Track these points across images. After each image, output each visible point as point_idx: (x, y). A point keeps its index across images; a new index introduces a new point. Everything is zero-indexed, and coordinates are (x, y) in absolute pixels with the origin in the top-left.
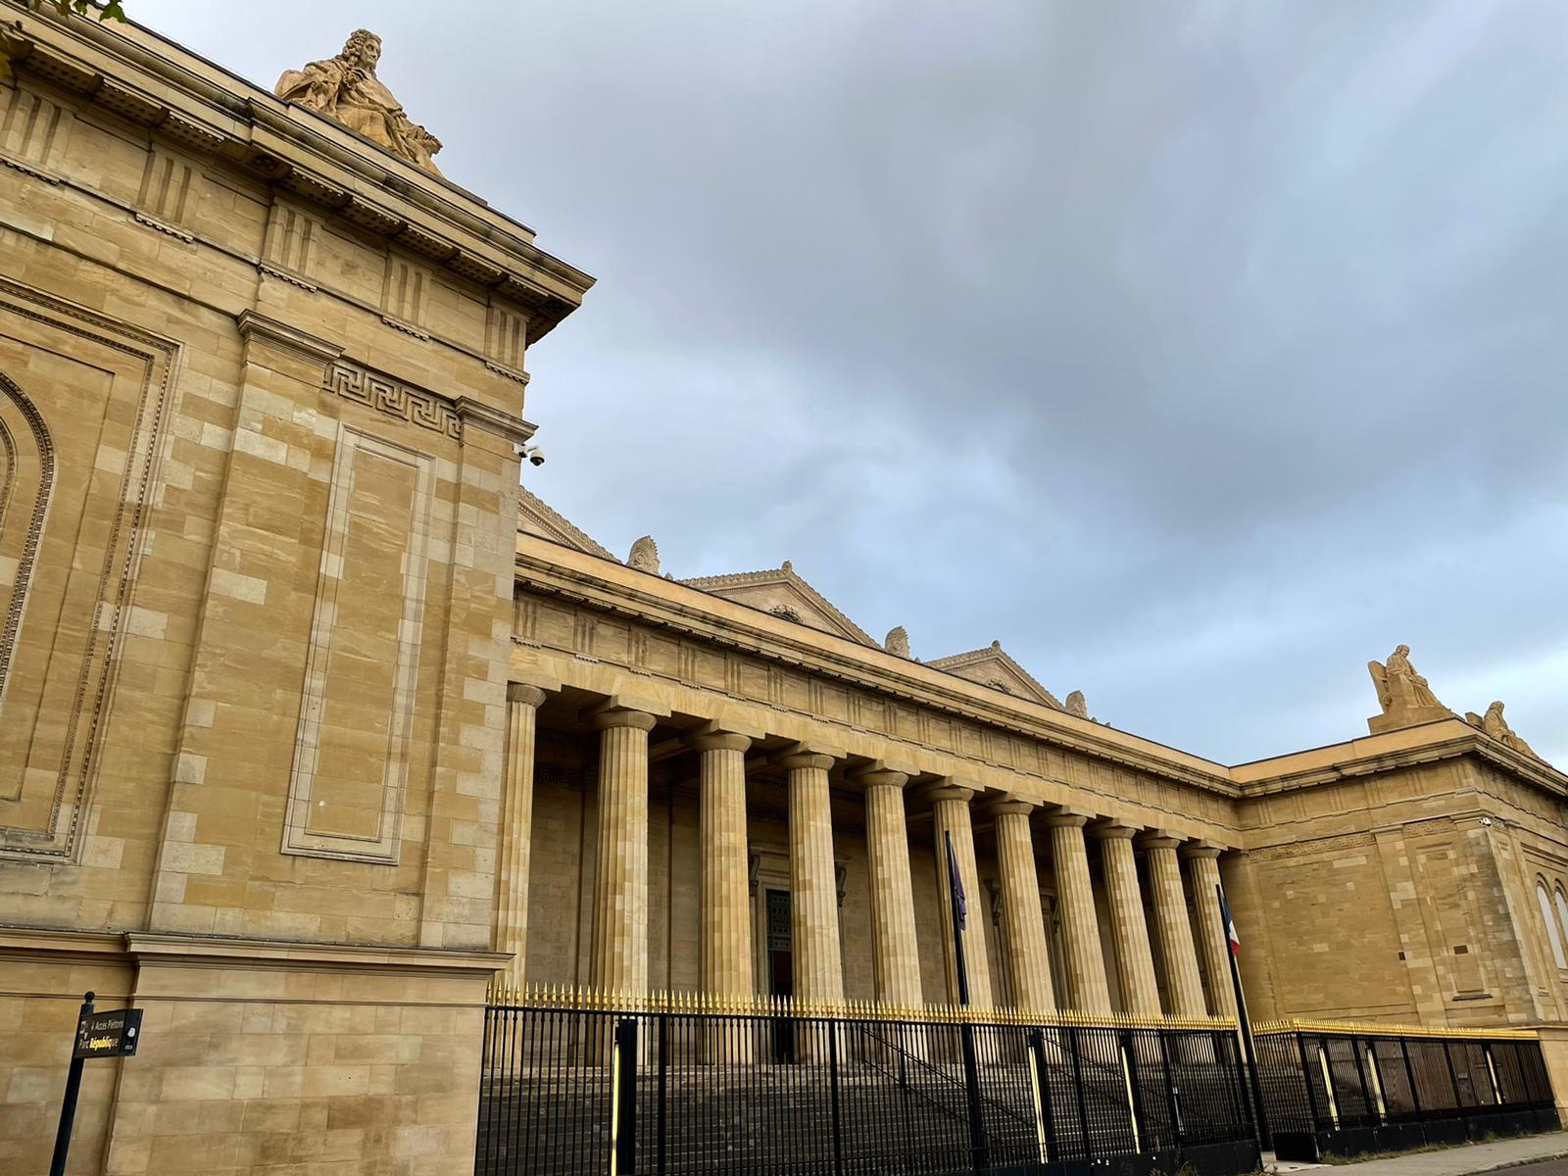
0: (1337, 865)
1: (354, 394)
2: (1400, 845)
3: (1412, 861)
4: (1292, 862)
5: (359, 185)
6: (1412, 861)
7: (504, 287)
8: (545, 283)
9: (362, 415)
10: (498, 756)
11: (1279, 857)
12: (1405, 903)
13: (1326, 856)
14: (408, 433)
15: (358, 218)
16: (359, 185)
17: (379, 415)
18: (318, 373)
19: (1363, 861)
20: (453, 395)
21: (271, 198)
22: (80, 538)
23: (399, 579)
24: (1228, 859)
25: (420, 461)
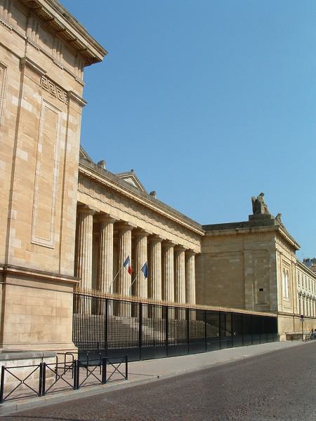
0: (230, 261)
1: (45, 87)
2: (251, 257)
3: (253, 262)
4: (216, 259)
5: (57, 15)
6: (253, 262)
7: (83, 52)
8: (95, 52)
9: (46, 95)
10: (72, 213)
11: (213, 256)
12: (249, 275)
13: (228, 258)
14: (55, 102)
15: (52, 25)
16: (57, 15)
17: (50, 95)
18: (38, 79)
19: (238, 260)
20: (68, 89)
21: (30, 14)
22: (13, 146)
23: (53, 155)
24: (197, 256)
25: (59, 112)
